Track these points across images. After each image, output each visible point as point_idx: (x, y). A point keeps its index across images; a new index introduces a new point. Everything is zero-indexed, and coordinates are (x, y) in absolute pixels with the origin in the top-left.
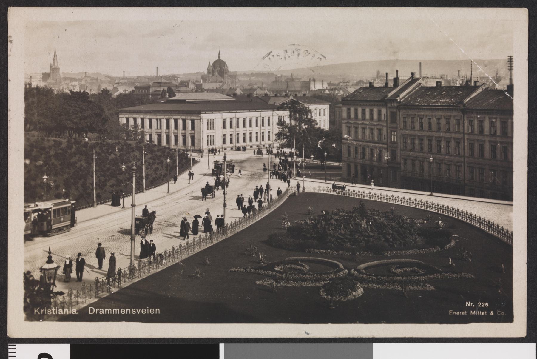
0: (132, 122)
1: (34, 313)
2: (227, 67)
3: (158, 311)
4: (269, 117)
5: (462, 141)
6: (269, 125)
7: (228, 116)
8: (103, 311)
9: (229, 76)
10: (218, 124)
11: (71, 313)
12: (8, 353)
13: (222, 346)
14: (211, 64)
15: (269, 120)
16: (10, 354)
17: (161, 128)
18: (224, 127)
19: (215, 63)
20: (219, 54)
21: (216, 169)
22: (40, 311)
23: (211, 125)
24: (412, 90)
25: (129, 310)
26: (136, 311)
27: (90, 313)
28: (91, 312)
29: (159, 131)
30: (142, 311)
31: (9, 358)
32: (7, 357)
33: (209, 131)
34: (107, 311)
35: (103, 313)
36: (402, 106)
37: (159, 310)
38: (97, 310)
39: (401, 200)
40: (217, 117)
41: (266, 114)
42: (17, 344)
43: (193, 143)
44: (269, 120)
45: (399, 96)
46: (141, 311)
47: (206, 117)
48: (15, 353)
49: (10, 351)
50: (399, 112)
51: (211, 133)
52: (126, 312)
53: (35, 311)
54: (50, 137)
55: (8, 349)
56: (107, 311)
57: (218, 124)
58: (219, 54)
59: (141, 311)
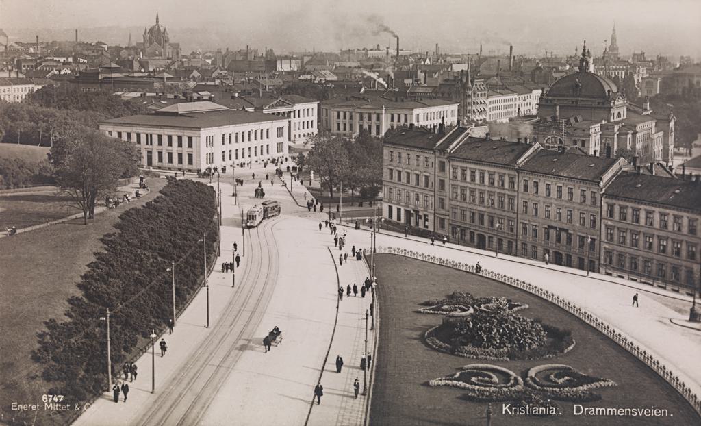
0: (125, 137)
1: (502, 412)
2: (167, 34)
3: (665, 412)
4: (268, 129)
8: (593, 410)
9: (170, 44)
14: (148, 31)
15: (267, 132)
19: (151, 30)
20: (157, 19)
23: (210, 142)
27: (575, 413)
29: (149, 146)
33: (209, 148)
34: (610, 411)
35: (593, 414)
37: (666, 411)
40: (217, 132)
43: (191, 162)
44: (267, 132)
45: (448, 147)
46: (644, 411)
47: (205, 133)
50: (450, 162)
51: (209, 150)
52: (624, 413)
53: (504, 409)
56: (610, 411)
58: (157, 19)
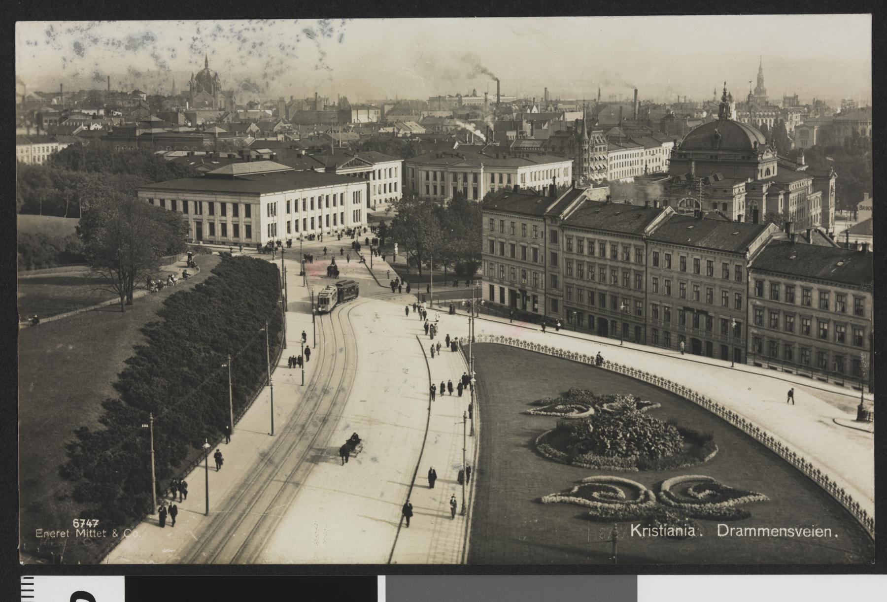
3: (828, 532)
4: (342, 194)
5: (644, 274)
6: (342, 204)
7: (294, 195)
8: (741, 531)
10: (281, 208)
11: (815, 536)
12: (20, 590)
13: (382, 580)
16: (23, 594)
17: (201, 213)
18: (288, 211)
21: (716, 446)
22: (640, 529)
23: (272, 210)
24: (571, 211)
25: (754, 529)
26: (795, 532)
28: (721, 533)
30: (804, 532)
31: (23, 599)
32: (19, 597)
36: (567, 225)
38: (732, 529)
39: (680, 390)
40: (280, 198)
41: (338, 189)
42: (36, 577)
43: (249, 234)
46: (802, 533)
47: (265, 199)
48: (33, 590)
49: (23, 587)
52: (779, 533)
53: (633, 530)
54: (704, 457)
55: (20, 584)
57: (281, 208)
59: (802, 533)
